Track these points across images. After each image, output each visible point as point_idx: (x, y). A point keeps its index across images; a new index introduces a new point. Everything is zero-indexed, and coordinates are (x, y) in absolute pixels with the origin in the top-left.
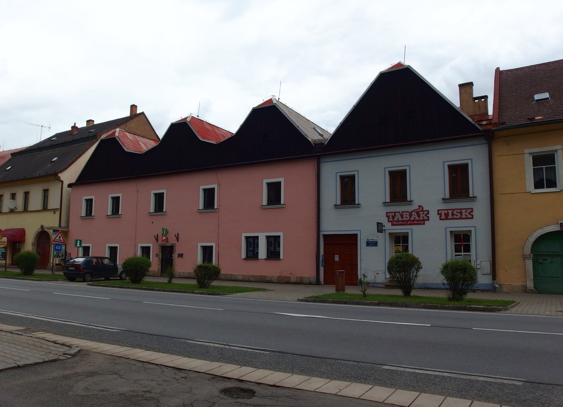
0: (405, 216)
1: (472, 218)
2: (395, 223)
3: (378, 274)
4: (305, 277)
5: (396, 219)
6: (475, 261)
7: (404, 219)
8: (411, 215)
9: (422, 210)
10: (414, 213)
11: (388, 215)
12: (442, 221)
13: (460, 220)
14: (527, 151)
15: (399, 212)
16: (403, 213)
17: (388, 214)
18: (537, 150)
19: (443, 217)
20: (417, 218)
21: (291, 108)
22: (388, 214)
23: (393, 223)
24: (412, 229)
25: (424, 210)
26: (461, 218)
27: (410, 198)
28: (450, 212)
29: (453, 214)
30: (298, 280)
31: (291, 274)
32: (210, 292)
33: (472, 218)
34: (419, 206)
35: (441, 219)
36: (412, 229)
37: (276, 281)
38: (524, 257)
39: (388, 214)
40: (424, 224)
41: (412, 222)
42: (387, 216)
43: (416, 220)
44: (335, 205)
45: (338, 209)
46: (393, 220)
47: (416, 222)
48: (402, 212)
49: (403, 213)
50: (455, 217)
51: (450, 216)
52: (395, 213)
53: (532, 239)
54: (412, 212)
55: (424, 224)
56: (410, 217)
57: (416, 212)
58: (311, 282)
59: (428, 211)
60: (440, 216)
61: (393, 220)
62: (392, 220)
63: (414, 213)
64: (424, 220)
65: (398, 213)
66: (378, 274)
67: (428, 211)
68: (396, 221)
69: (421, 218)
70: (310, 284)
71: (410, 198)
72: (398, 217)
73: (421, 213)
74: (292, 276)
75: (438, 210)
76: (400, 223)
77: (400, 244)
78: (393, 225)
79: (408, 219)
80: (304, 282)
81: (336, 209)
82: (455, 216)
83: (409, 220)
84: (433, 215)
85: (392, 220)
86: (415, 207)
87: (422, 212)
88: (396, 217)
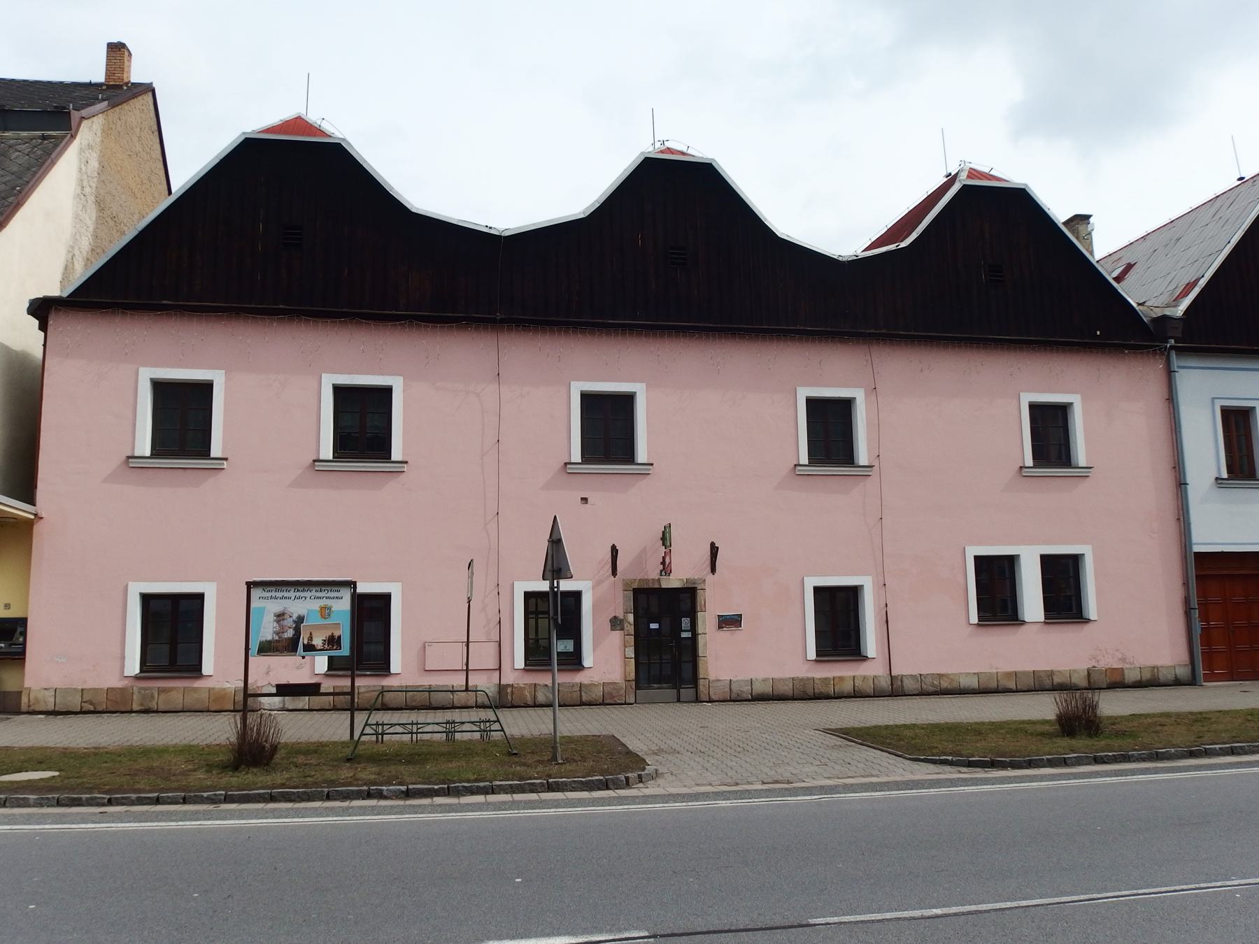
4: (1162, 667)
30: (1147, 676)
58: (1178, 677)
70: (1177, 683)
74: (1127, 666)
80: (1162, 679)
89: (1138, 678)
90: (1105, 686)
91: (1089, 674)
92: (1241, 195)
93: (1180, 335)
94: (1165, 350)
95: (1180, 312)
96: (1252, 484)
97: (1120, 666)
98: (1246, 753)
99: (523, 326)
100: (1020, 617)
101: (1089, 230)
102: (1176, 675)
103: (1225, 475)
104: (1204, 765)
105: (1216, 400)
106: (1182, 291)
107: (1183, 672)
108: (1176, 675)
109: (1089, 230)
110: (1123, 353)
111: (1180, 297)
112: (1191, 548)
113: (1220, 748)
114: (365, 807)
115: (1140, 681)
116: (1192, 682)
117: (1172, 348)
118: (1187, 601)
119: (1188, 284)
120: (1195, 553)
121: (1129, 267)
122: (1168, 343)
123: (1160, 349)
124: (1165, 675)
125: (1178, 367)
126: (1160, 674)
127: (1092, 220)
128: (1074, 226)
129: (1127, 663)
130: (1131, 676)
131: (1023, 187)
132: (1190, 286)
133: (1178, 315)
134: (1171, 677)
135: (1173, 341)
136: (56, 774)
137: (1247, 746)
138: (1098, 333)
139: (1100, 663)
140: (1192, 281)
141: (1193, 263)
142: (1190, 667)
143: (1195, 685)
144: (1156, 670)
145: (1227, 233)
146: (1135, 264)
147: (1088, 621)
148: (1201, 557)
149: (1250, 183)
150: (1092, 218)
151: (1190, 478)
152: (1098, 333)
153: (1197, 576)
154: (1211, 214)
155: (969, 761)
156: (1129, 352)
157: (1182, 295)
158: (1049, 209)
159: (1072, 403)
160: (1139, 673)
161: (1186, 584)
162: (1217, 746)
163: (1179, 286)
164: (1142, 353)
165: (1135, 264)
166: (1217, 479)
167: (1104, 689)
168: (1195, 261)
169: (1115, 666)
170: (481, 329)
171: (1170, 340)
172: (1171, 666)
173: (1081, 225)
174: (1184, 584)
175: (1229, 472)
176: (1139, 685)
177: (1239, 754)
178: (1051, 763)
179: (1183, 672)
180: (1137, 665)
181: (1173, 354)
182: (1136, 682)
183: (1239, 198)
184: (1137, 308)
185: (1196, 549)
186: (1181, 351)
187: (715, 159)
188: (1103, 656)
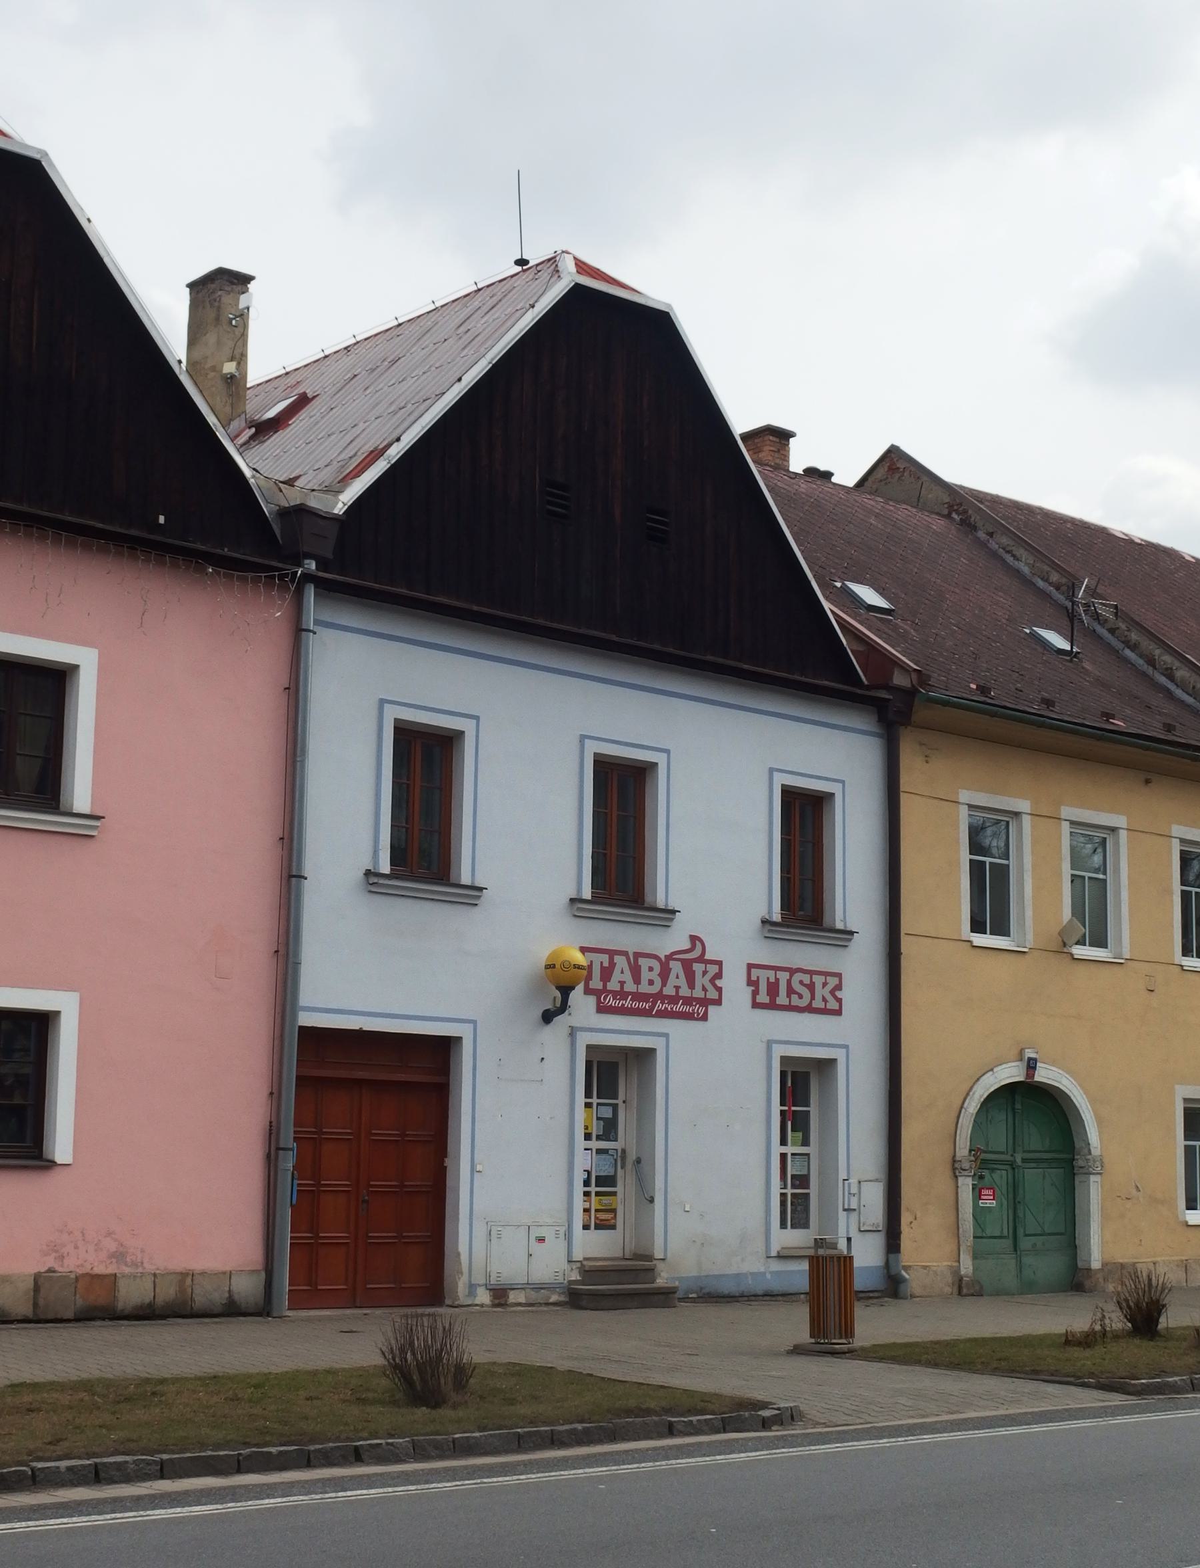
0: (645, 975)
1: (838, 1012)
2: (611, 1001)
3: (541, 1240)
4: (203, 1273)
5: (613, 985)
6: (846, 1182)
7: (644, 988)
8: (665, 974)
9: (701, 959)
10: (676, 967)
11: (754, 978)
12: (759, 1012)
13: (806, 1015)
14: (965, 796)
15: (625, 953)
16: (641, 961)
17: (753, 970)
18: (982, 799)
19: (763, 998)
20: (685, 992)
21: (432, 307)
22: (753, 970)
23: (605, 998)
24: (666, 1035)
25: (707, 957)
26: (809, 1009)
27: (473, 875)
28: (783, 977)
29: (790, 991)
30: (167, 1293)
31: (119, 1256)
32: (338, 1439)
33: (838, 1012)
34: (694, 939)
35: (756, 1005)
36: (666, 1035)
37: (25, 1309)
38: (955, 1168)
39: (755, 973)
40: (705, 1018)
41: (669, 1003)
42: (750, 982)
43: (682, 998)
44: (572, 900)
45: (383, 898)
46: (605, 986)
47: (679, 1007)
48: (638, 955)
49: (641, 961)
50: (795, 1001)
51: (782, 999)
52: (611, 953)
53: (973, 1106)
54: (670, 957)
55: (705, 1018)
56: (664, 984)
57: (683, 961)
58: (236, 1297)
59: (719, 963)
60: (753, 991)
61: (605, 986)
62: (600, 986)
63: (676, 967)
64: (705, 1002)
65: (624, 958)
66: (541, 1240)
67: (719, 963)
68: (615, 994)
69: (698, 994)
70: (232, 1310)
71: (473, 875)
72: (622, 975)
73: (698, 968)
74: (127, 1270)
75: (750, 967)
76: (628, 1003)
77: (598, 1098)
78: (602, 1009)
79: (654, 989)
80: (200, 1301)
81: (573, 918)
82: (796, 996)
83: (659, 996)
84: (734, 985)
85: (600, 986)
86: (673, 940)
87: (703, 966)
88: (616, 976)
89: (148, 1298)
90: (70, 1314)
91: (37, 1288)
92: (514, 292)
93: (330, 555)
94: (292, 581)
95: (340, 505)
96: (648, 917)
97: (111, 1270)
98: (127, 1479)
99: (197, 562)
100: (47, 1154)
101: (241, 306)
102: (230, 1296)
103: (385, 868)
104: (79, 1503)
105: (386, 706)
106: (362, 462)
107: (247, 1287)
108: (230, 1296)
109: (241, 306)
110: (203, 571)
111: (351, 476)
112: (294, 1017)
113: (69, 1469)
114: (594, 1455)
115: (151, 1305)
116: (264, 1309)
117: (308, 577)
118: (272, 1132)
119: (372, 452)
120: (300, 1027)
121: (303, 401)
122: (300, 565)
123: (281, 578)
124: (207, 1294)
125: (317, 622)
126: (197, 1290)
127: (252, 286)
128: (213, 292)
129: (126, 1265)
130: (132, 1294)
131: (37, 156)
132: (376, 454)
133: (336, 511)
134: (218, 1298)
135: (312, 565)
136: (419, 1388)
137: (134, 1461)
138: (162, 519)
139: (66, 1261)
140: (381, 447)
141: (395, 413)
142: (263, 1274)
143: (268, 1315)
144: (189, 1281)
145: (466, 361)
146: (314, 397)
147: (51, 1164)
148: (311, 1036)
149: (533, 271)
150: (252, 282)
151: (310, 866)
152: (162, 519)
153: (299, 1078)
154: (458, 321)
155: (454, 1440)
156: (218, 573)
157: (354, 473)
158: (89, 220)
159: (76, 667)
160: (150, 1286)
161: (275, 1095)
162: (64, 1464)
163: (359, 453)
164: (243, 580)
165: (314, 397)
166: (368, 873)
167: (68, 1321)
168: (400, 409)
169: (100, 1269)
170: (49, 541)
171: (307, 561)
172: (224, 1273)
173: (229, 293)
174: (271, 1094)
175: (394, 862)
176: (147, 1314)
177: (112, 1481)
178: (76, 1478)
179: (247, 1287)
180: (149, 1268)
181: (310, 591)
182: (141, 1307)
183: (511, 294)
184: (252, 481)
185: (307, 1019)
186: (327, 588)
187: (49, 152)
188: (76, 1247)
